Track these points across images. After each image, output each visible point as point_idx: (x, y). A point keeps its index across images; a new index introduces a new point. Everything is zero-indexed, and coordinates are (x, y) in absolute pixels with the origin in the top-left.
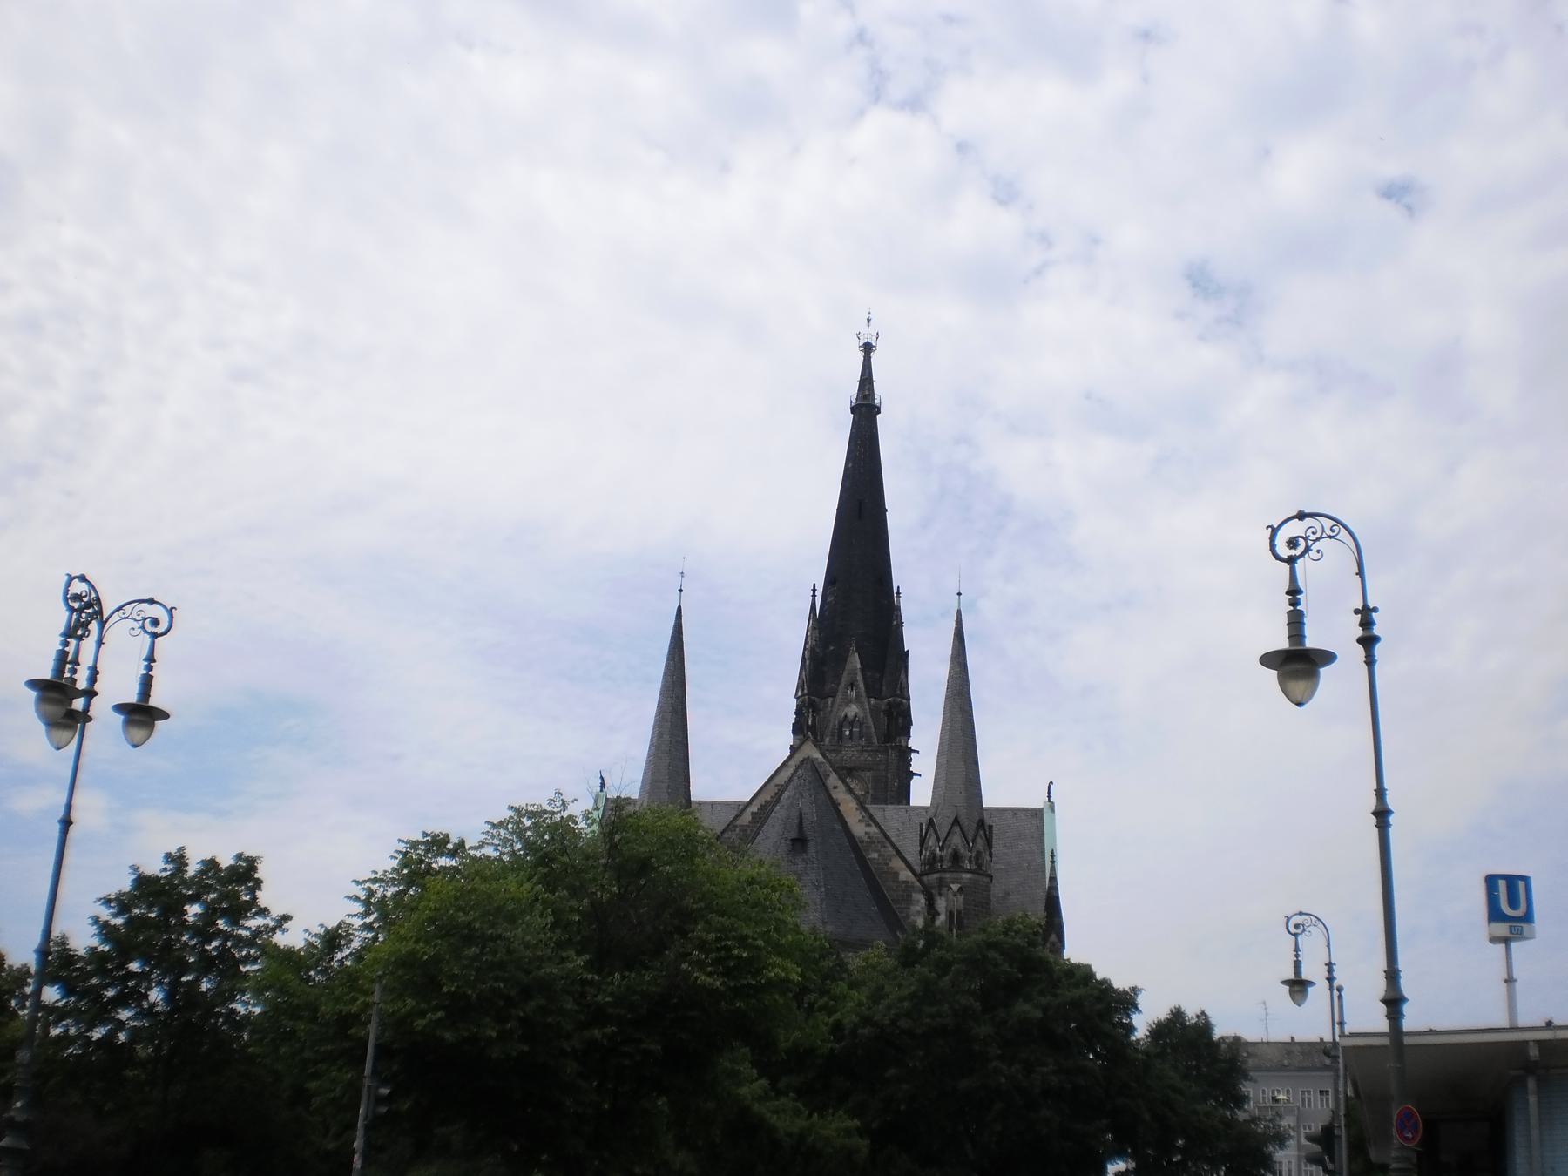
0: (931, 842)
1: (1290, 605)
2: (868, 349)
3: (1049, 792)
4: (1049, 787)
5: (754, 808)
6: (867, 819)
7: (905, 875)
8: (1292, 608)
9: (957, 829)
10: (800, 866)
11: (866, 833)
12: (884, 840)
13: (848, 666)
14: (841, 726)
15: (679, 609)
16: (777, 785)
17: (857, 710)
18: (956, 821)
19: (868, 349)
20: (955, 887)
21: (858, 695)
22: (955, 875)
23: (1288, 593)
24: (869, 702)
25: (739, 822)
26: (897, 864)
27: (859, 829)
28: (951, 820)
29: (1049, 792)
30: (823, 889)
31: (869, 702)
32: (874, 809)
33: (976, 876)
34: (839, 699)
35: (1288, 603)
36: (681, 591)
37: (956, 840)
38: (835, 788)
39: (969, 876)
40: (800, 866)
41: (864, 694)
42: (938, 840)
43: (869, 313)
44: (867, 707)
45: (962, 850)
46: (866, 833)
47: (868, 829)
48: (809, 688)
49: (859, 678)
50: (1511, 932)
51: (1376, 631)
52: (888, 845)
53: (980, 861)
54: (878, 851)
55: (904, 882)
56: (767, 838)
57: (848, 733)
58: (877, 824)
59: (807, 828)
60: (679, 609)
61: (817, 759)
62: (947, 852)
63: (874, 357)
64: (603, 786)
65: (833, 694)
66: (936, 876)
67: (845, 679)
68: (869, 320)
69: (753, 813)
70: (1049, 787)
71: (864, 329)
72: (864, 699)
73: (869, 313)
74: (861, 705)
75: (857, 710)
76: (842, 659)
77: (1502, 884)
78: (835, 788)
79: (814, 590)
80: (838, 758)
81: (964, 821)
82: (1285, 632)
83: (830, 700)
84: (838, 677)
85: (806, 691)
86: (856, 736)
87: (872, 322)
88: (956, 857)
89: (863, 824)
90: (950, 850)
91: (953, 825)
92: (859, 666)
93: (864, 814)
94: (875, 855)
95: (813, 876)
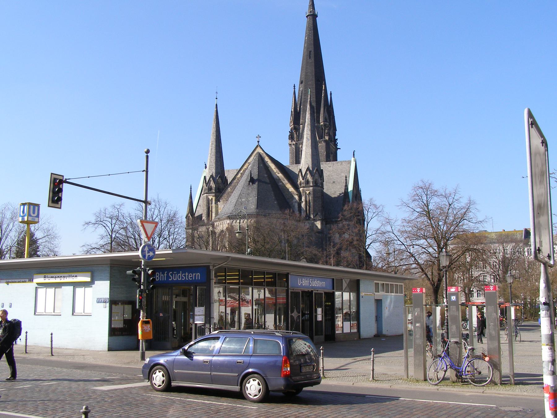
4: (354, 152)
70: (354, 152)
79: (294, 86)
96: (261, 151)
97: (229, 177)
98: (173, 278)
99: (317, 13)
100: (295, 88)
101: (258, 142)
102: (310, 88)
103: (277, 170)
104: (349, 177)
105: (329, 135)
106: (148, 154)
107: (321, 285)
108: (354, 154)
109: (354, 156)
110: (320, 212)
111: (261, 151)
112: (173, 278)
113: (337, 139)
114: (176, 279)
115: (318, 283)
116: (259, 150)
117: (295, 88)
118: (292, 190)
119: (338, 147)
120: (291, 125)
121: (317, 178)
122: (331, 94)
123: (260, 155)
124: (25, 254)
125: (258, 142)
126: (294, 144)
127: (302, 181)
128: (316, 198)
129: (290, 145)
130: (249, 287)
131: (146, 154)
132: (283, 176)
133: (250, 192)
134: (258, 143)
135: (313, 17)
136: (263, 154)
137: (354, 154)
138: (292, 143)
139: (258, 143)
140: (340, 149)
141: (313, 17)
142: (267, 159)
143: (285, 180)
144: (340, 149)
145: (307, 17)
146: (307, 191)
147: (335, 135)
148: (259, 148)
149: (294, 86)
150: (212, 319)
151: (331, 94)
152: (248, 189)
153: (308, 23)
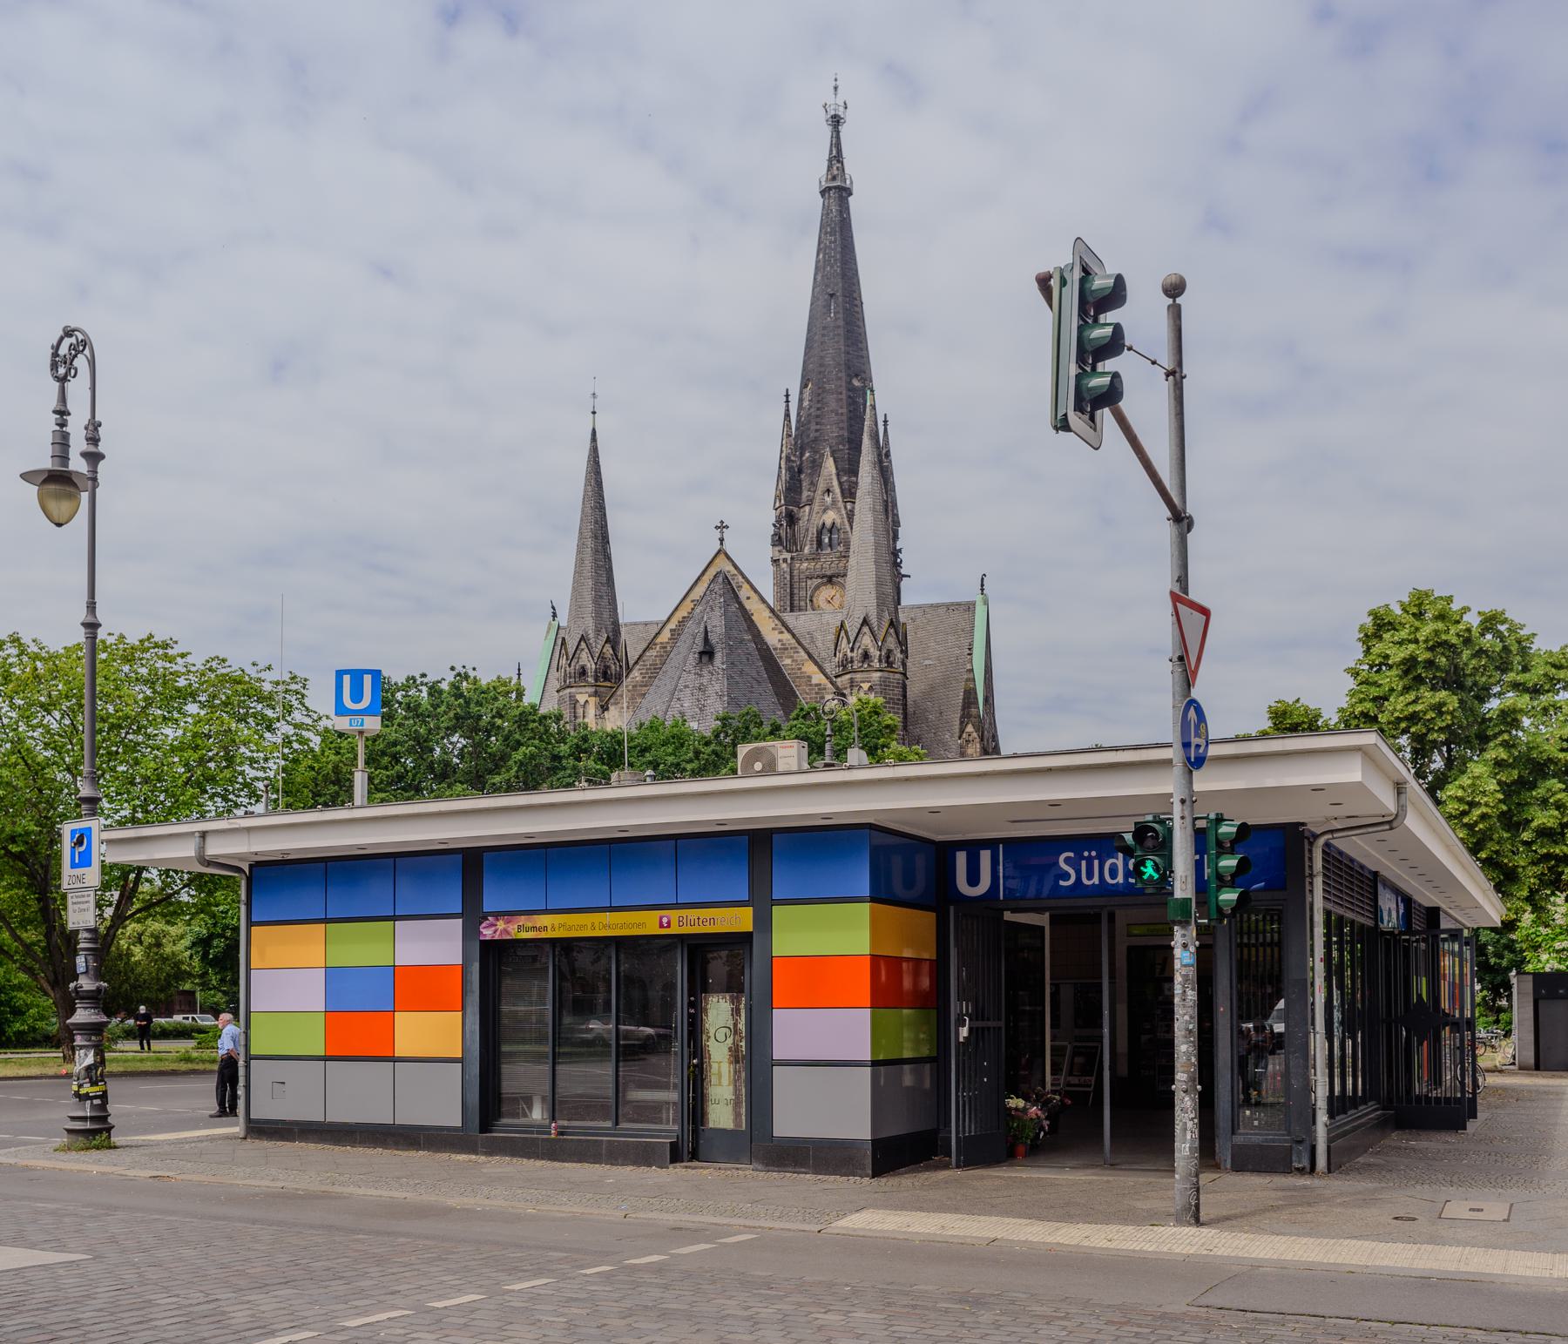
0: (844, 644)
1: (57, 424)
2: (836, 121)
3: (982, 585)
4: (982, 579)
5: (672, 625)
6: (780, 626)
7: (818, 678)
8: (58, 428)
9: (866, 629)
10: (707, 676)
11: (779, 641)
12: (797, 645)
13: (824, 472)
14: (820, 533)
15: (594, 432)
16: (693, 601)
17: (835, 516)
18: (865, 622)
19: (836, 121)
20: (866, 686)
21: (834, 502)
22: (865, 675)
23: (55, 412)
24: (845, 508)
25: (659, 640)
26: (810, 668)
27: (772, 636)
28: (861, 621)
29: (982, 585)
30: (726, 698)
31: (845, 508)
32: (789, 618)
33: (886, 674)
34: (816, 507)
35: (54, 422)
36: (594, 413)
37: (867, 641)
38: (748, 598)
39: (879, 674)
40: (707, 676)
41: (840, 499)
42: (849, 643)
43: (836, 80)
44: (844, 512)
45: (872, 650)
46: (779, 641)
47: (781, 637)
48: (785, 498)
49: (835, 483)
50: (351, 725)
51: (102, 448)
52: (801, 650)
53: (891, 659)
54: (791, 657)
55: (817, 685)
56: (679, 653)
57: (827, 540)
58: (789, 630)
59: (713, 638)
60: (594, 432)
61: (729, 572)
62: (857, 654)
63: (843, 129)
64: (554, 615)
65: (810, 502)
66: (848, 676)
67: (821, 486)
68: (836, 88)
69: (671, 630)
70: (982, 579)
71: (830, 100)
72: (841, 504)
73: (836, 80)
74: (839, 510)
75: (835, 516)
76: (816, 465)
77: (347, 679)
78: (748, 598)
79: (787, 396)
80: (817, 566)
81: (874, 621)
82: (49, 450)
83: (807, 508)
84: (813, 484)
85: (783, 502)
86: (835, 542)
87: (839, 90)
88: (866, 656)
89: (776, 632)
90: (860, 651)
91: (862, 625)
92: (834, 471)
93: (777, 622)
94: (788, 661)
95: (717, 687)
96: (729, 568)
97: (632, 645)
98: (1078, 873)
99: (852, 183)
100: (787, 401)
101: (722, 540)
106: (1178, 300)
109: (982, 590)
111: (729, 568)
112: (1078, 873)
113: (900, 551)
114: (1096, 880)
116: (722, 565)
117: (787, 401)
120: (777, 505)
121: (892, 646)
125: (722, 540)
126: (785, 560)
127: (849, 654)
128: (889, 703)
129: (775, 562)
131: (1170, 301)
134: (722, 544)
135: (837, 193)
138: (782, 557)
139: (722, 544)
141: (837, 193)
145: (823, 193)
148: (722, 556)
149: (787, 396)
150: (925, 1051)
153: (826, 211)
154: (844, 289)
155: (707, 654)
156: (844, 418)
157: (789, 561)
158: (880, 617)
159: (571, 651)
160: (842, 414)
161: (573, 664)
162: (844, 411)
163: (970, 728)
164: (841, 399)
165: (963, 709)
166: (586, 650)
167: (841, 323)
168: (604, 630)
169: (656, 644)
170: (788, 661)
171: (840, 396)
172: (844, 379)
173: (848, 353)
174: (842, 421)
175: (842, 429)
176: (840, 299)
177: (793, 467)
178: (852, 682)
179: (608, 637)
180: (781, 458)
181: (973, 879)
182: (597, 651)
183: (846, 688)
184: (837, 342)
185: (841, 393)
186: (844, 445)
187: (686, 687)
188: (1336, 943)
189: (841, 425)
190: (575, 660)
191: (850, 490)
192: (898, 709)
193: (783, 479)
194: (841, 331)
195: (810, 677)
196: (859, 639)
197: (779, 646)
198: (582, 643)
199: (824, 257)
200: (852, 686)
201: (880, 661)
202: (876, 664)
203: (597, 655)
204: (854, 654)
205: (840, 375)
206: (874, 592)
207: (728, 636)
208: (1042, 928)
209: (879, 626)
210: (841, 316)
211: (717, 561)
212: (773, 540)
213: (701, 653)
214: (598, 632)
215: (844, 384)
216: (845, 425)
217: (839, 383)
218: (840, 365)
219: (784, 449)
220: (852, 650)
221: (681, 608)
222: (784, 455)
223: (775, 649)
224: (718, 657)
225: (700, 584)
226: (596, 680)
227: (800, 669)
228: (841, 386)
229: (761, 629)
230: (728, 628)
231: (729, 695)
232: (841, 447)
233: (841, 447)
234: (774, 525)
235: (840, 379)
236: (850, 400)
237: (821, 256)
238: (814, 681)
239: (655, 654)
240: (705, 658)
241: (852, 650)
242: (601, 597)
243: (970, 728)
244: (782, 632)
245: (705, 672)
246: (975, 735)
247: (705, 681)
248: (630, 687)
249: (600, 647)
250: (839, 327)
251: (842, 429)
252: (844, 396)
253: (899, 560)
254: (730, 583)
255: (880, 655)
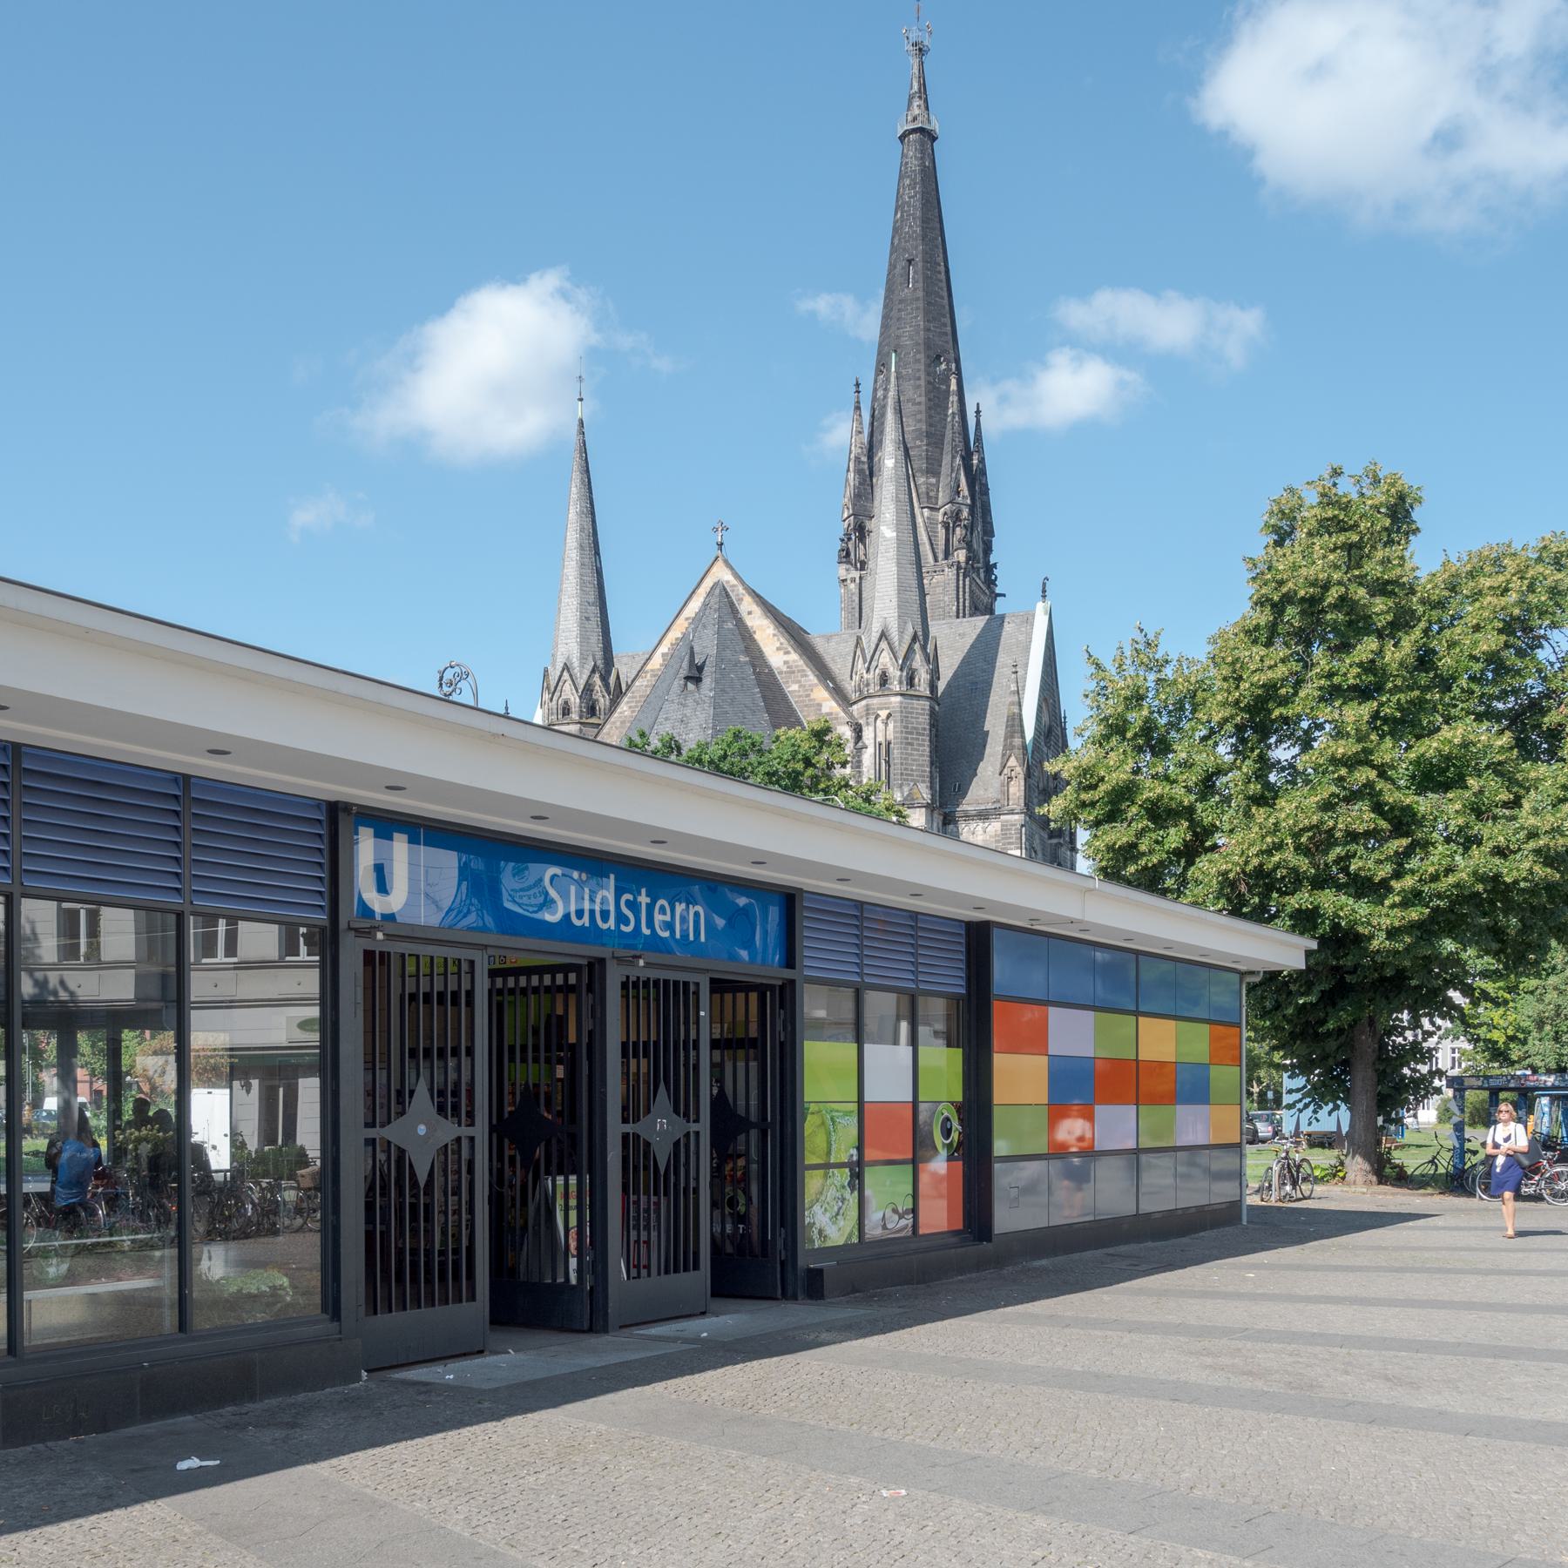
0: (860, 666)
4: (1044, 584)
9: (884, 645)
16: (687, 619)
24: (922, 514)
25: (649, 667)
28: (878, 635)
31: (922, 514)
37: (885, 659)
38: (750, 613)
39: (898, 699)
42: (864, 663)
47: (786, 658)
54: (799, 682)
61: (728, 582)
62: (873, 676)
66: (864, 703)
69: (663, 655)
70: (1044, 584)
78: (750, 613)
79: (858, 385)
81: (894, 634)
89: (782, 652)
94: (795, 687)
96: (727, 577)
102: (895, 351)
103: (782, 640)
104: (1026, 665)
105: (969, 547)
107: (669, 926)
108: (1044, 591)
110: (923, 782)
113: (995, 565)
115: (633, 906)
116: (721, 573)
118: (831, 708)
119: (998, 590)
120: (846, 515)
122: (978, 412)
123: (721, 591)
124: (1247, 1066)
125: (721, 545)
126: (853, 580)
128: (911, 733)
130: (137, 999)
132: (802, 662)
133: (688, 712)
136: (734, 586)
137: (1044, 591)
138: (849, 576)
140: (1004, 595)
142: (747, 606)
143: (809, 673)
144: (1004, 595)
146: (881, 709)
147: (988, 549)
148: (720, 564)
149: (858, 385)
151: (978, 412)
152: (684, 705)
154: (925, 252)
155: (695, 676)
156: (923, 408)
157: (857, 581)
158: (901, 632)
159: (553, 684)
160: (919, 403)
161: (555, 698)
162: (923, 399)
163: (1013, 762)
164: (919, 386)
165: (1005, 740)
166: (569, 682)
167: (920, 294)
168: (591, 658)
169: (647, 672)
170: (795, 687)
171: (918, 382)
172: (923, 361)
173: (929, 330)
174: (920, 412)
175: (920, 421)
176: (920, 265)
177: (863, 470)
178: (868, 710)
179: (595, 665)
180: (850, 460)
181: (697, 914)
182: (581, 683)
183: (862, 717)
184: (916, 317)
185: (919, 379)
186: (922, 441)
187: (666, 719)
188: (303, 935)
189: (919, 417)
190: (557, 694)
191: (928, 493)
192: (923, 740)
193: (852, 484)
194: (921, 304)
195: (820, 705)
196: (876, 657)
197: (785, 669)
198: (565, 673)
199: (902, 216)
200: (868, 714)
201: (900, 683)
202: (895, 686)
203: (582, 687)
204: (870, 676)
205: (918, 356)
206: (895, 600)
207: (720, 658)
208: (298, 955)
209: (900, 641)
210: (920, 285)
211: (714, 569)
212: (840, 557)
213: (687, 678)
214: (583, 658)
215: (923, 367)
216: (923, 416)
217: (917, 366)
218: (918, 344)
219: (853, 448)
220: (868, 670)
221: (674, 627)
222: (852, 456)
223: (780, 673)
224: (708, 681)
225: (695, 598)
226: (581, 717)
227: (808, 696)
228: (919, 370)
229: (764, 650)
230: (721, 647)
231: (714, 728)
232: (918, 443)
233: (918, 443)
234: (842, 540)
235: (918, 361)
236: (931, 386)
237: (899, 215)
238: (825, 710)
239: (645, 683)
240: (691, 686)
241: (868, 670)
242: (588, 619)
243: (1013, 762)
244: (787, 653)
245: (690, 702)
246: (1018, 769)
247: (688, 712)
248: (618, 724)
249: (585, 677)
250: (918, 299)
251: (920, 421)
252: (922, 382)
253: (993, 577)
254: (728, 596)
255: (901, 676)
